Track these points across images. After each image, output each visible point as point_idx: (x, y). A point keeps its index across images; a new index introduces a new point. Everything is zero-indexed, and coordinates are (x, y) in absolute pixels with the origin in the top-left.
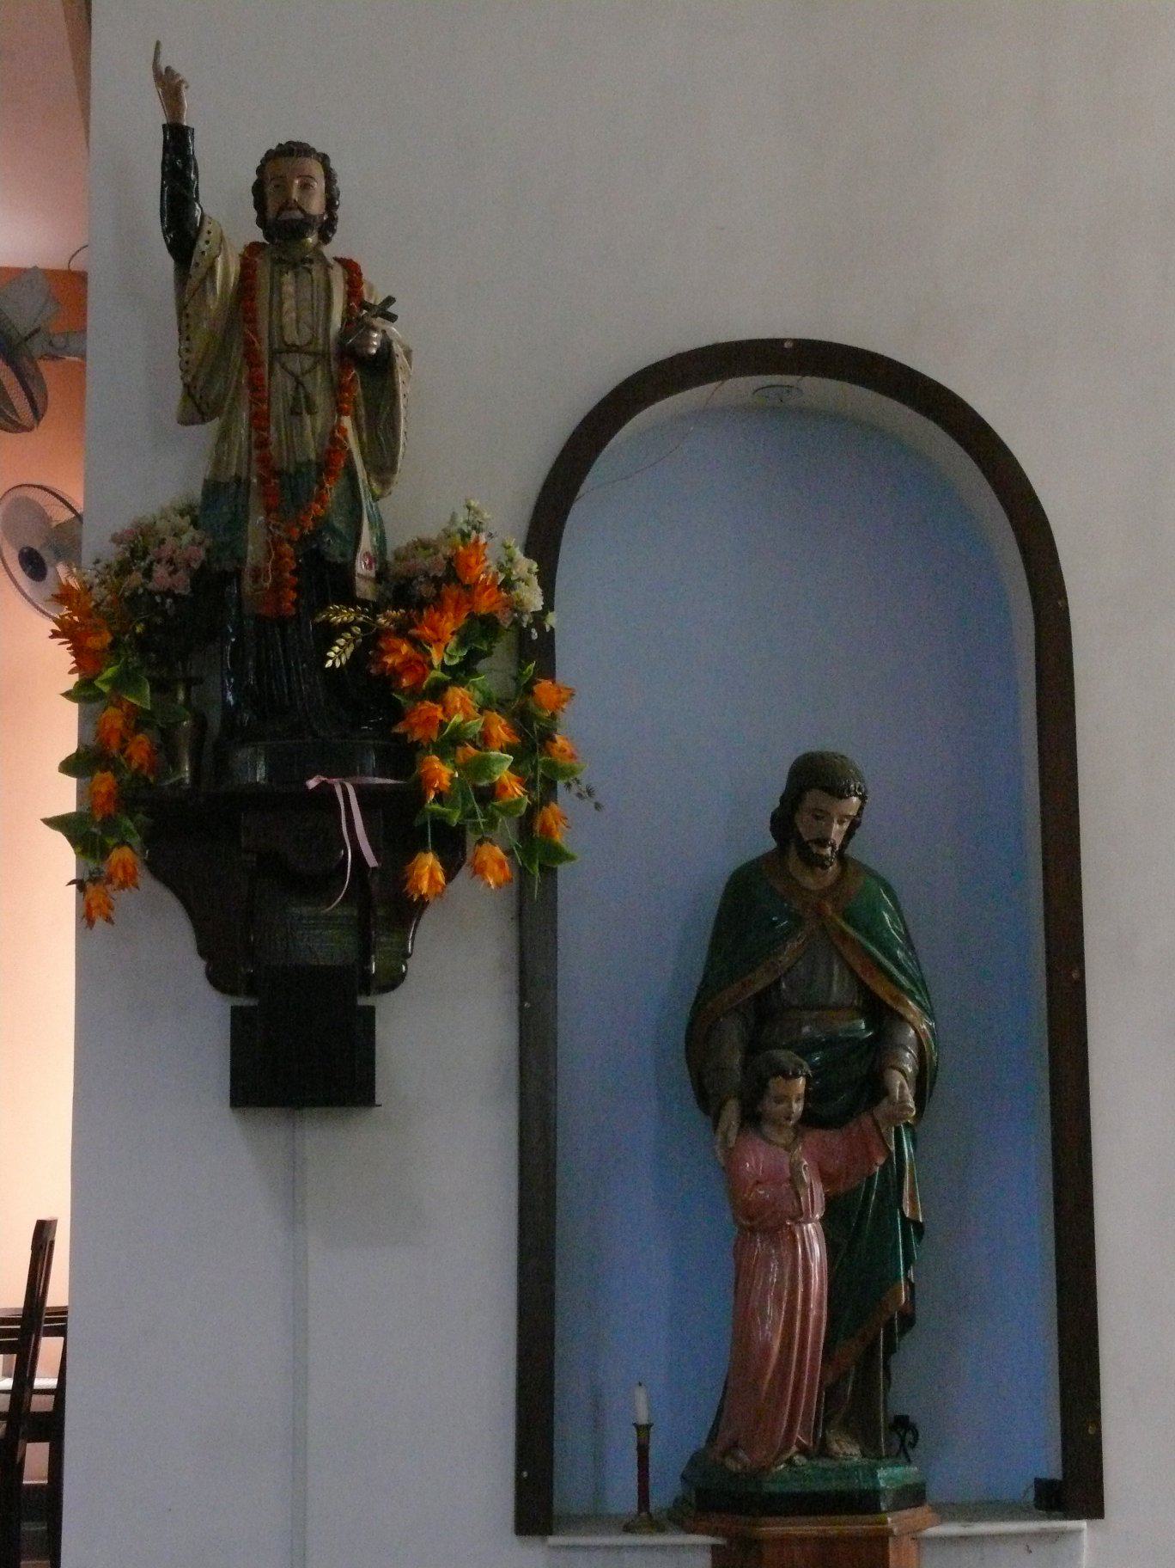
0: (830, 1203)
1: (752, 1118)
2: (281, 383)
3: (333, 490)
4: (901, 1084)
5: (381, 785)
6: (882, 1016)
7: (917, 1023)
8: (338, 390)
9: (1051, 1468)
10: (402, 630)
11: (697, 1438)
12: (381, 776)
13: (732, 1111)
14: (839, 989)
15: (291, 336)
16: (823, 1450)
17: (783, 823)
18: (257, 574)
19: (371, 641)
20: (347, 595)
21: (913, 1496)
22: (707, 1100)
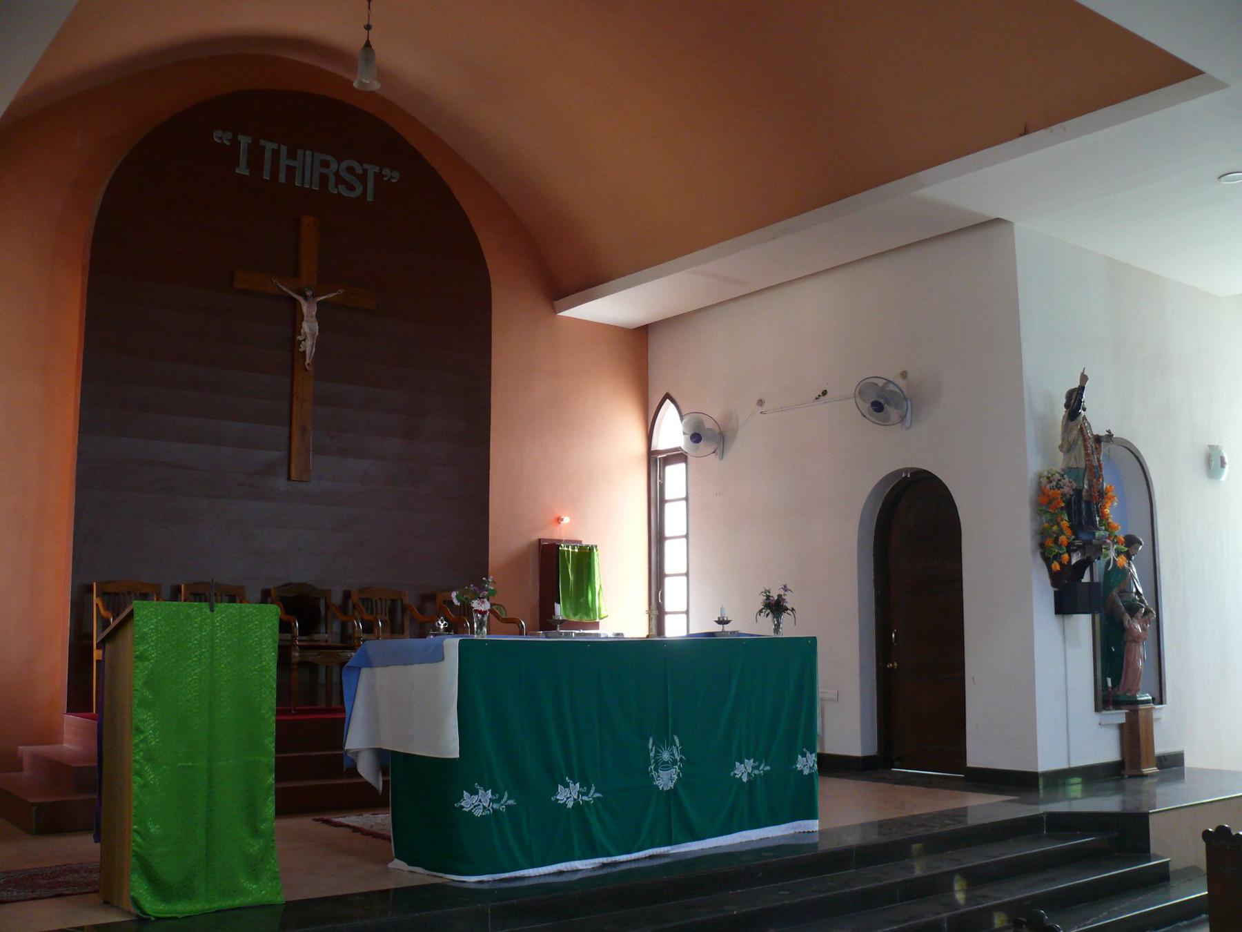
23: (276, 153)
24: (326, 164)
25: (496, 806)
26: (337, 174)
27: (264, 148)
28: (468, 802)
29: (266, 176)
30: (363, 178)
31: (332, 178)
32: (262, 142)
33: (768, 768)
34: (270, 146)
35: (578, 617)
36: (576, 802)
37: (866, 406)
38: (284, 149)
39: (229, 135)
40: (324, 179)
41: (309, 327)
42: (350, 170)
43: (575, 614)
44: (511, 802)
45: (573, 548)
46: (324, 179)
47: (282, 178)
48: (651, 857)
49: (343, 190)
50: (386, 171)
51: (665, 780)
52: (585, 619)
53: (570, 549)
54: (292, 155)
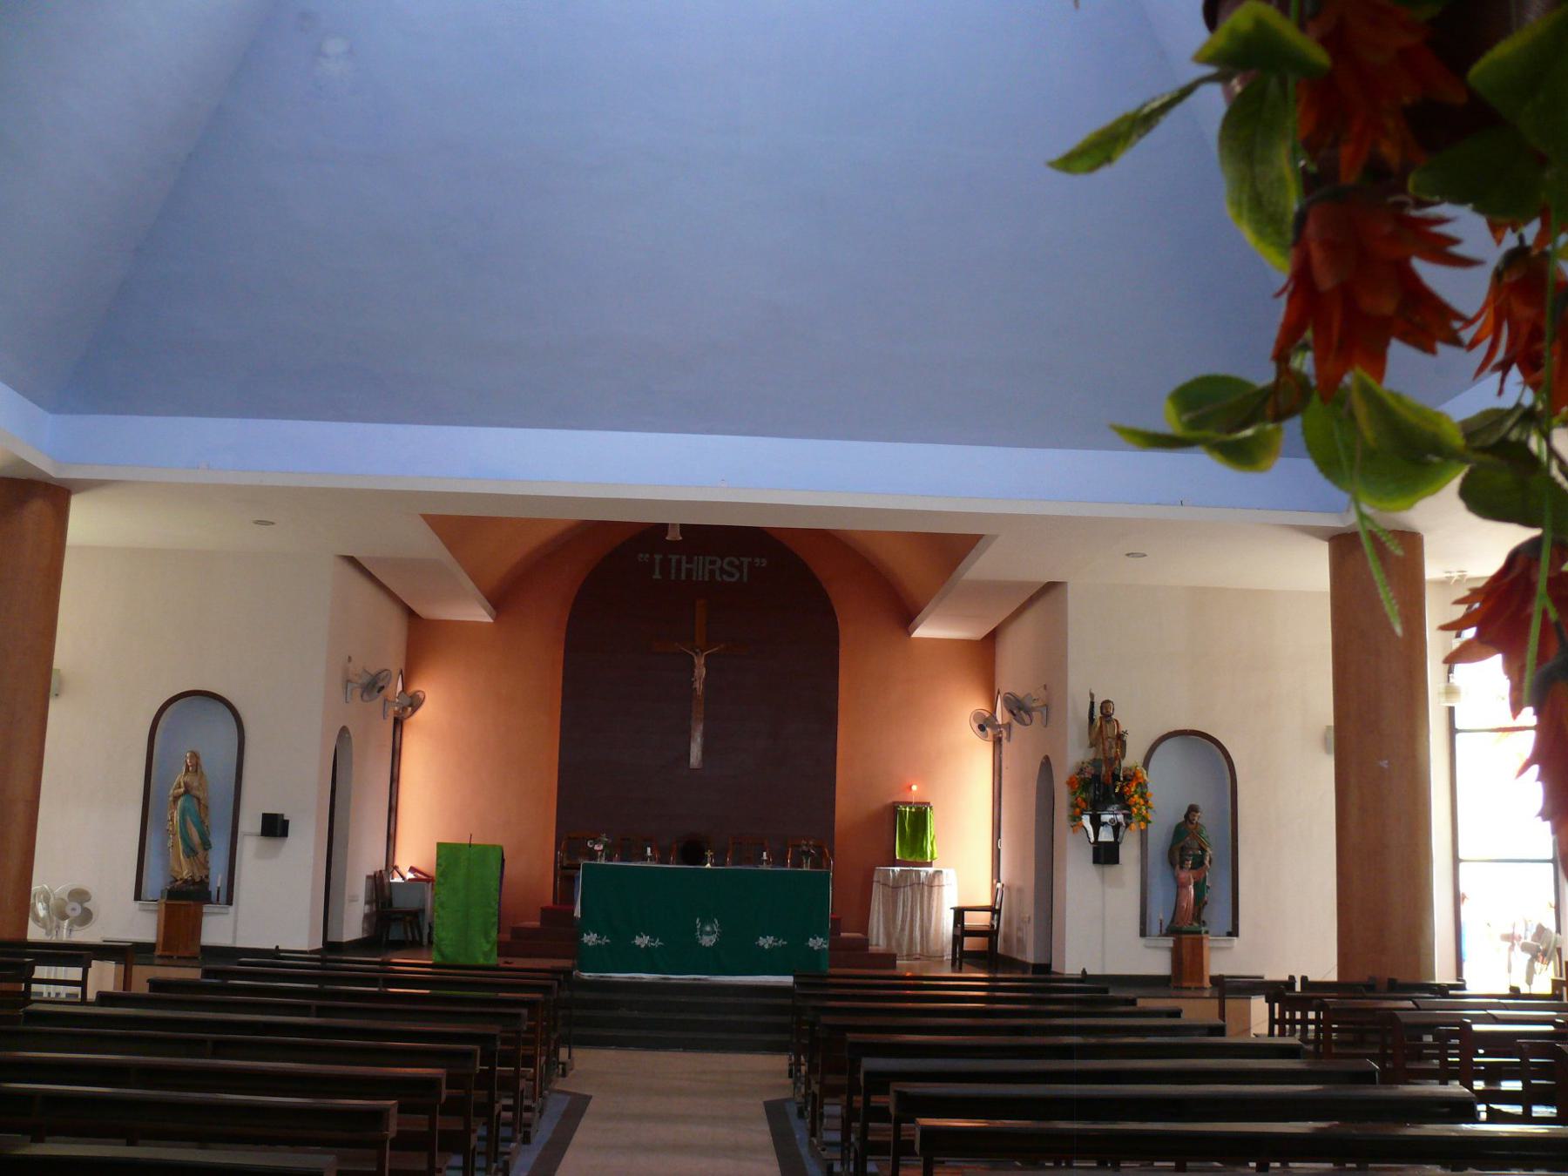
0: (1195, 882)
1: (1182, 868)
2: (1107, 744)
3: (1117, 762)
4: (1207, 862)
5: (8, 970)
6: (1203, 850)
7: (1209, 851)
8: (1117, 744)
9: (1230, 930)
10: (1127, 785)
11: (1168, 923)
12: (677, 864)
13: (1178, 867)
14: (1196, 846)
15: (1110, 735)
16: (1191, 924)
17: (1187, 816)
18: (1104, 776)
19: (1121, 788)
20: (1120, 781)
21: (1207, 932)
22: (1172, 864)
23: (679, 562)
24: (713, 563)
25: (599, 942)
26: (721, 569)
27: (671, 559)
28: (586, 938)
29: (673, 577)
30: (740, 568)
31: (717, 573)
32: (670, 556)
33: (785, 943)
34: (674, 558)
35: (914, 857)
36: (646, 946)
37: (975, 726)
38: (684, 558)
39: (647, 556)
40: (712, 572)
41: (701, 671)
42: (731, 564)
43: (910, 856)
44: (608, 941)
45: (911, 808)
46: (712, 572)
47: (683, 577)
48: (695, 979)
49: (725, 577)
50: (757, 560)
51: (708, 941)
52: (919, 860)
53: (908, 809)
54: (689, 561)
